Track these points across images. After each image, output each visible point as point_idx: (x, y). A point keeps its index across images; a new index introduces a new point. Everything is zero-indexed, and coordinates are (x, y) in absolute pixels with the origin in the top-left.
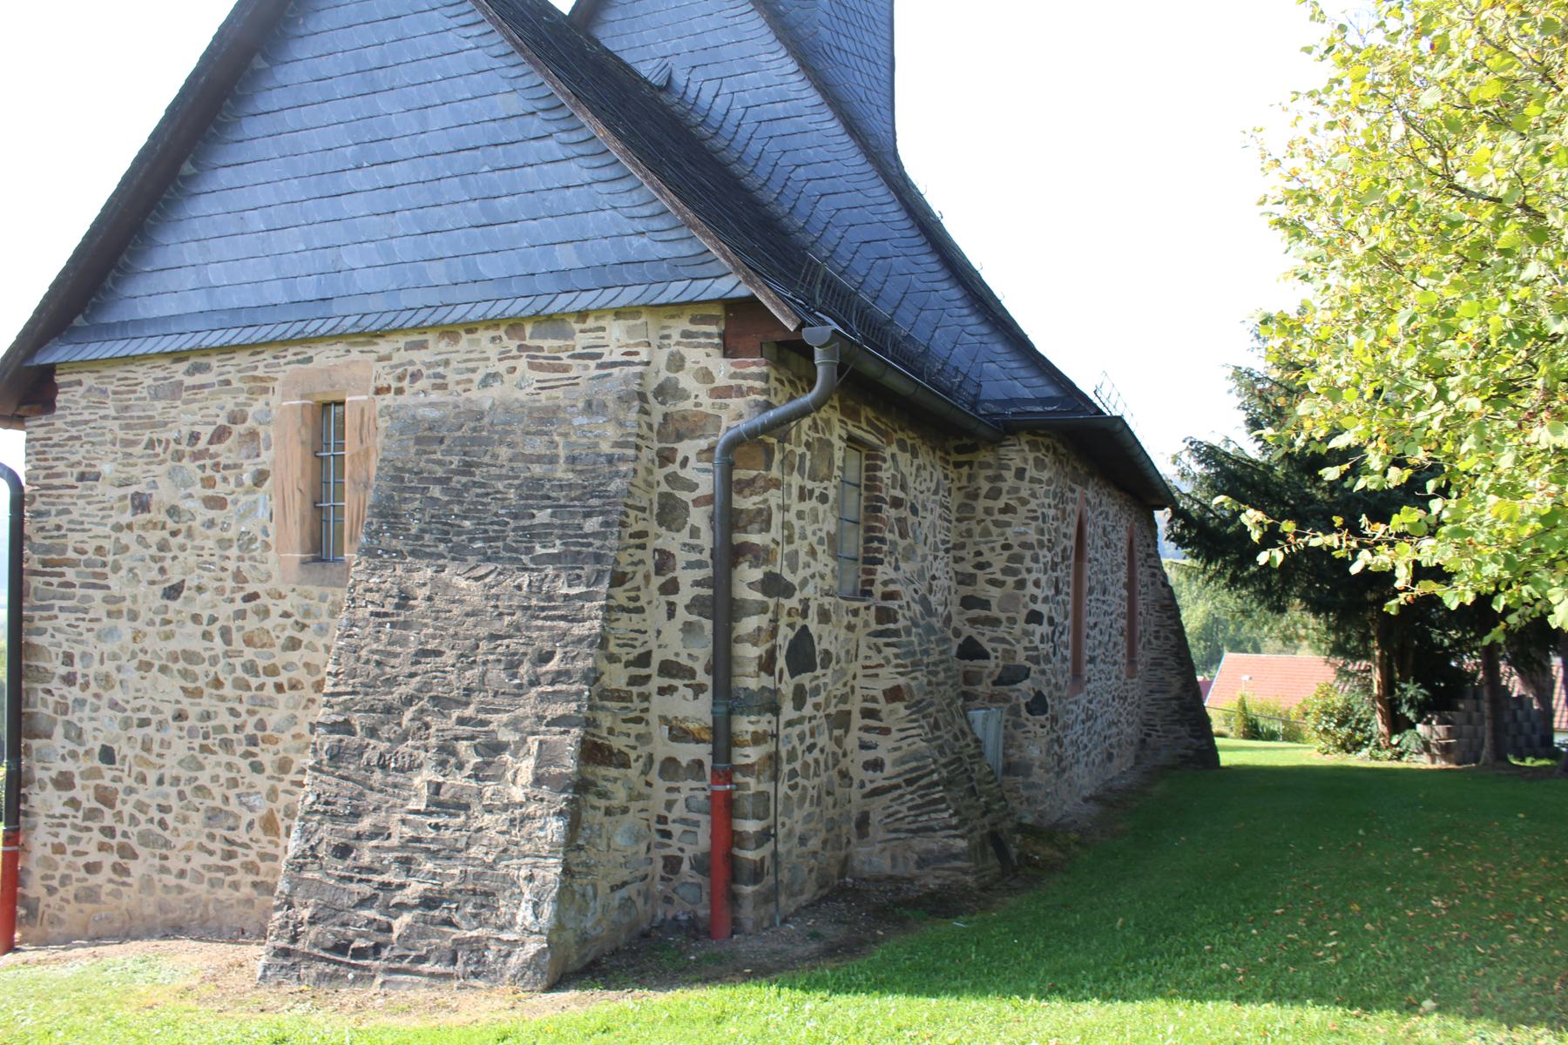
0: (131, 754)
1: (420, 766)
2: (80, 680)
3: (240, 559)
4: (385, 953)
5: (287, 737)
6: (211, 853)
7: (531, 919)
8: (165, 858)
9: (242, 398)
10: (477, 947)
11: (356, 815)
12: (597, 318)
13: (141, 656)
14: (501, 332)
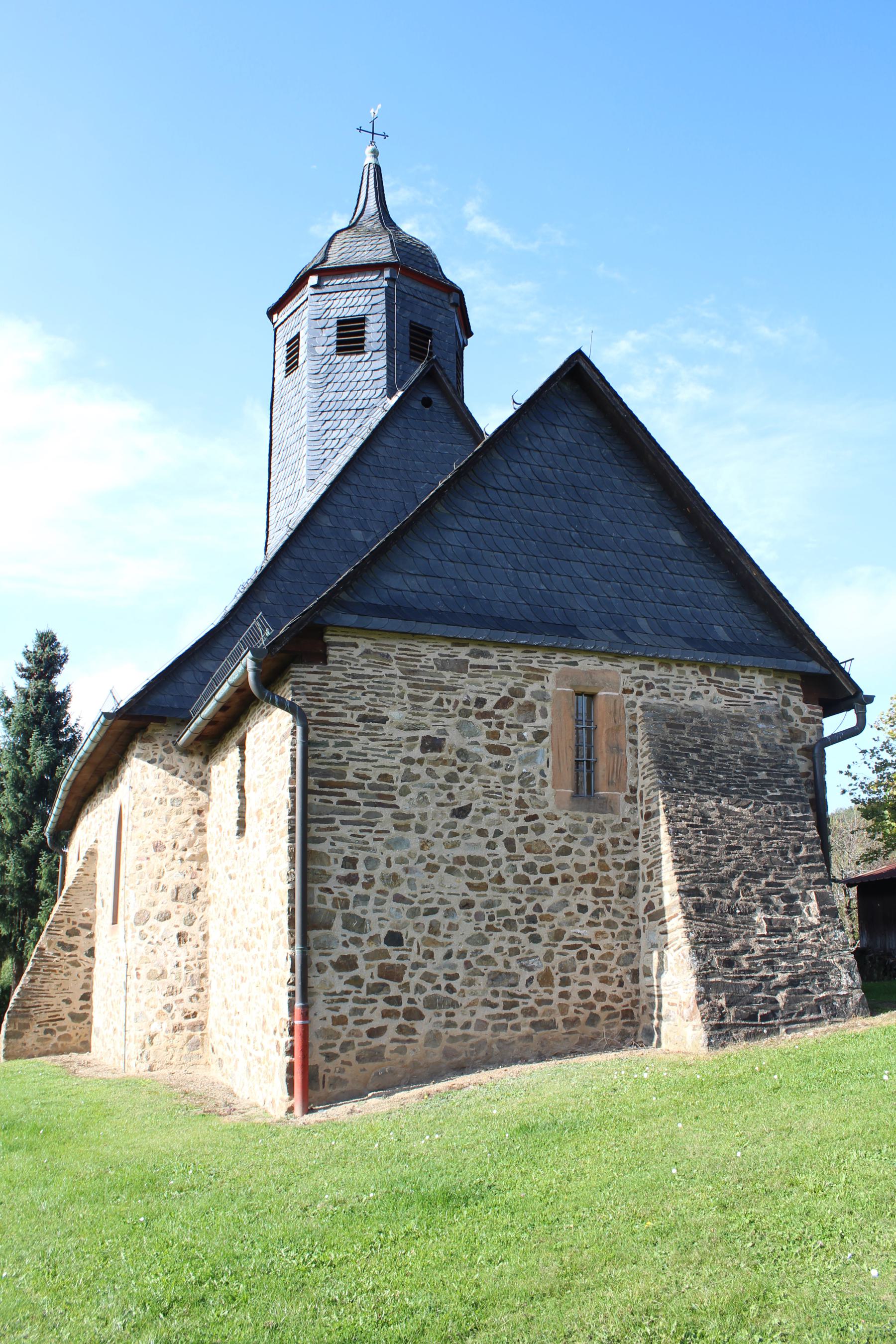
0: (418, 937)
1: (755, 910)
2: (362, 879)
3: (522, 791)
4: (779, 1015)
5: (561, 915)
6: (494, 1006)
7: (851, 982)
8: (452, 1014)
9: (520, 680)
10: (827, 1001)
11: (727, 942)
12: (752, 672)
13: (429, 860)
14: (697, 669)
